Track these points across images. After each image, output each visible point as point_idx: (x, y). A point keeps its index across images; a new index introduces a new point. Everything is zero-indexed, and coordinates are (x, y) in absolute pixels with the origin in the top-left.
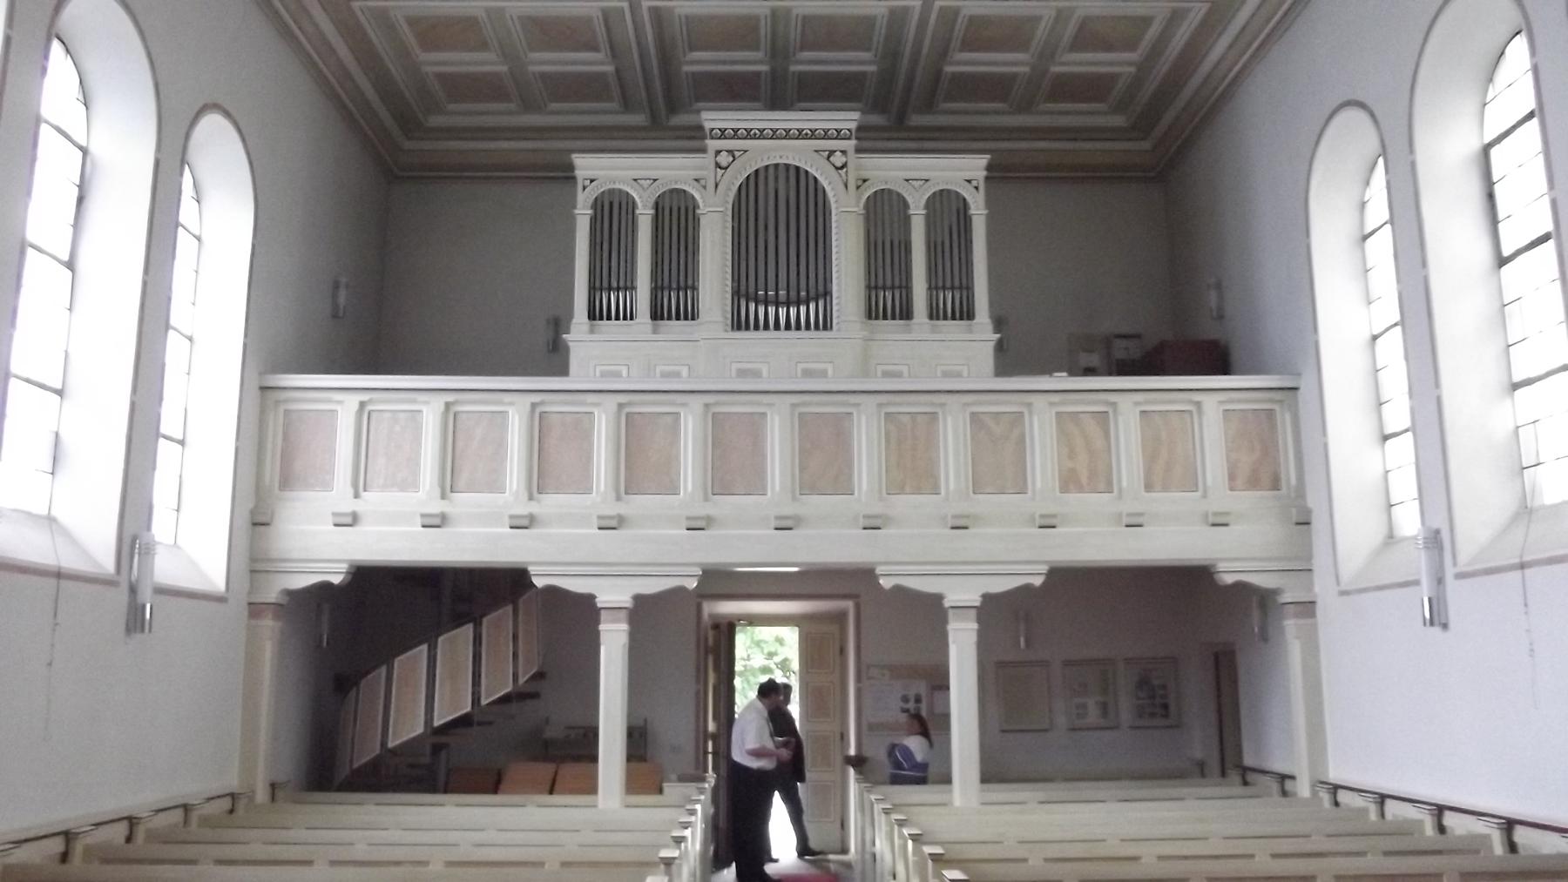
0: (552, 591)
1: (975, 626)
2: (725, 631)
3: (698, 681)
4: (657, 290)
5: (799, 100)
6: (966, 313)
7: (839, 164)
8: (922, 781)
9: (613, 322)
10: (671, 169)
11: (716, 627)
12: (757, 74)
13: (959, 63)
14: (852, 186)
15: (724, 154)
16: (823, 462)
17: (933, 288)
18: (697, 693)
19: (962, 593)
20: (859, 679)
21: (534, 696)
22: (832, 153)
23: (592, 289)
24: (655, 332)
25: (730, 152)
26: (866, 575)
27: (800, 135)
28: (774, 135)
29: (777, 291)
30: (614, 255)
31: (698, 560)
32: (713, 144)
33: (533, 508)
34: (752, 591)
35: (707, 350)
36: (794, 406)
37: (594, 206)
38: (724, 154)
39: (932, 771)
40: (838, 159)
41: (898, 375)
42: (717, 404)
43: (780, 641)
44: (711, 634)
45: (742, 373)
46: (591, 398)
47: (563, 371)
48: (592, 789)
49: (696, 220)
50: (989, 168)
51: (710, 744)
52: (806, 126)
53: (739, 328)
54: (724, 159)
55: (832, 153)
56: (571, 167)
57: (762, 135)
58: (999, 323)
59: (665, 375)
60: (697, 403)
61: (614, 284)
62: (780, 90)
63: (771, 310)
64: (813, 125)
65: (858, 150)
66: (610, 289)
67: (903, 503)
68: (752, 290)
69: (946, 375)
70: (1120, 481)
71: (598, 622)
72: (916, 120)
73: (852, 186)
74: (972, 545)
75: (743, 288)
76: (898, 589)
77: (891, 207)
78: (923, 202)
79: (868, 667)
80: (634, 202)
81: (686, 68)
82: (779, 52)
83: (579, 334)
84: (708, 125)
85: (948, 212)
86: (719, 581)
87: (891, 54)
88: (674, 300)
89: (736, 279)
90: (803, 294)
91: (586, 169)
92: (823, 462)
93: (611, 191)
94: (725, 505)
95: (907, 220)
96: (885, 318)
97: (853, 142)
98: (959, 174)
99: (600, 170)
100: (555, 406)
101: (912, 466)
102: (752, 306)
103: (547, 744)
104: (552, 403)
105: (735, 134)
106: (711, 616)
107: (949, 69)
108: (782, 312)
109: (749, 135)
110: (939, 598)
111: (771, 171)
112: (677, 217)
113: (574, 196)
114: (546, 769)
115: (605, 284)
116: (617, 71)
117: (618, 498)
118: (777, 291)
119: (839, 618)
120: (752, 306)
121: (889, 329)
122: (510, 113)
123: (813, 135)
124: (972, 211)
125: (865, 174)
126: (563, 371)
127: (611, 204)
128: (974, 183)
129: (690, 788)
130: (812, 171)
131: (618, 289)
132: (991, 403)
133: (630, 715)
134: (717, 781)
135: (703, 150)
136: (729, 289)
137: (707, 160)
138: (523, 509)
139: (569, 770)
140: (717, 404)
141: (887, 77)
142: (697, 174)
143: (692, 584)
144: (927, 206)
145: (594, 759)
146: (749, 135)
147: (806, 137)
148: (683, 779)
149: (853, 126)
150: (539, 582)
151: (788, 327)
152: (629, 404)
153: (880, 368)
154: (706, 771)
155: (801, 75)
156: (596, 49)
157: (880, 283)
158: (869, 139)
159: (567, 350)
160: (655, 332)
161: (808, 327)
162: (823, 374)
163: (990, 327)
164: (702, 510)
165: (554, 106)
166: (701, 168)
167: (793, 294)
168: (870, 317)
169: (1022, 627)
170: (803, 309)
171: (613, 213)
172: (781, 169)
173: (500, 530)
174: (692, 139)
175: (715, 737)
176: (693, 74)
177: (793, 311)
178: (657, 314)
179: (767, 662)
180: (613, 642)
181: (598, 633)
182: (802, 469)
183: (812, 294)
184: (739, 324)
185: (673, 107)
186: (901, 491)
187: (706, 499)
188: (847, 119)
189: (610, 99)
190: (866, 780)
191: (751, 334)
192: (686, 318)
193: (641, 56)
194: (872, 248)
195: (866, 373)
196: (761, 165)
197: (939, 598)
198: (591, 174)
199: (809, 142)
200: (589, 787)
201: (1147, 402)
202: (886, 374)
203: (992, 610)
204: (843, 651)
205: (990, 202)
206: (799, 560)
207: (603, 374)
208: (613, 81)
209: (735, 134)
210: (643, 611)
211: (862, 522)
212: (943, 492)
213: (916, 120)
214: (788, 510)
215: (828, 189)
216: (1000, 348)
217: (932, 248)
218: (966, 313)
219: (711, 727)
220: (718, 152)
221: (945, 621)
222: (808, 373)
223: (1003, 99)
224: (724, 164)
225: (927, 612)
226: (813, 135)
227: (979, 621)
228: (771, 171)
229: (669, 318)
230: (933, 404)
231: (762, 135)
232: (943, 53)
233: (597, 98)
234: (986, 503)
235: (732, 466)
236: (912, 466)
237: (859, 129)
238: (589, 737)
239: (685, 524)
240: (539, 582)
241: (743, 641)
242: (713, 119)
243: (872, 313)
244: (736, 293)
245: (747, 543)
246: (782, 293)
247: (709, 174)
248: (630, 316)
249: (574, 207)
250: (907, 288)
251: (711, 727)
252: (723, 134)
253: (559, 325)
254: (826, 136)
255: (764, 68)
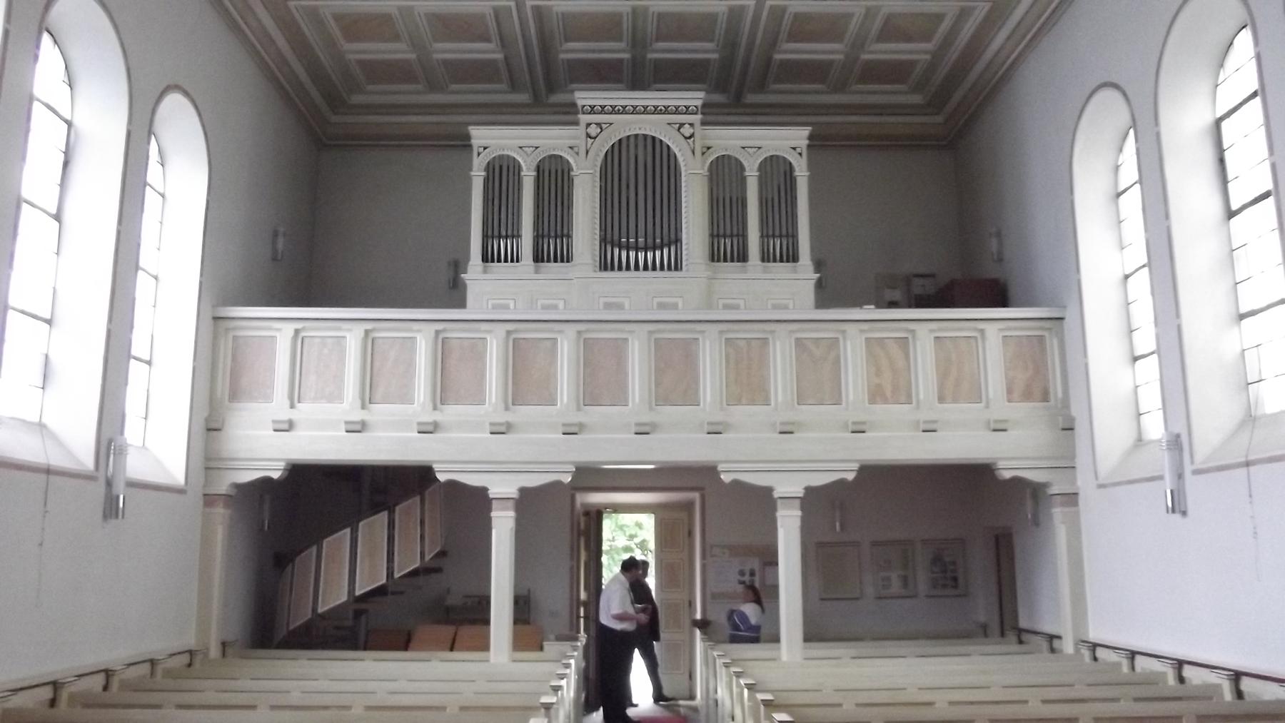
0: (452, 484)
1: (799, 513)
2: (594, 518)
3: (572, 558)
4: (538, 238)
5: (655, 82)
6: (792, 257)
7: (687, 135)
8: (755, 640)
9: (503, 264)
10: (549, 139)
11: (587, 514)
12: (621, 61)
13: (786, 52)
14: (698, 152)
15: (593, 126)
16: (675, 379)
17: (764, 236)
18: (572, 568)
19: (789, 486)
20: (704, 557)
21: (438, 570)
22: (682, 125)
23: (485, 237)
24: (537, 272)
25: (598, 124)
26: (710, 471)
27: (656, 111)
28: (635, 111)
29: (637, 239)
30: (503, 209)
31: (572, 459)
32: (584, 118)
33: (437, 416)
34: (616, 484)
35: (579, 287)
36: (650, 332)
37: (487, 169)
38: (593, 126)
39: (764, 632)
40: (687, 131)
41: (736, 307)
42: (587, 331)
43: (639, 525)
44: (582, 519)
45: (608, 306)
46: (484, 326)
47: (461, 304)
48: (485, 647)
49: (571, 180)
50: (811, 138)
51: (582, 610)
52: (661, 103)
53: (606, 269)
54: (593, 130)
55: (682, 125)
56: (468, 137)
57: (624, 111)
58: (819, 265)
59: (545, 307)
60: (571, 330)
61: (504, 233)
62: (639, 74)
63: (632, 254)
64: (666, 103)
65: (703, 123)
66: (500, 237)
67: (740, 413)
68: (616, 238)
69: (775, 307)
70: (918, 394)
71: (490, 510)
72: (751, 98)
73: (698, 152)
74: (796, 446)
75: (609, 236)
76: (736, 483)
77: (730, 169)
78: (757, 165)
79: (712, 547)
80: (520, 166)
81: (562, 56)
82: (639, 43)
83: (474, 274)
84: (580, 103)
85: (777, 173)
86: (589, 477)
87: (730, 44)
88: (552, 246)
89: (603, 229)
90: (658, 241)
91: (480, 138)
92: (675, 379)
93: (501, 157)
94: (594, 414)
95: (743, 180)
96: (725, 260)
97: (699, 117)
98: (786, 142)
99: (492, 140)
100: (455, 333)
101: (747, 382)
102: (616, 251)
103: (448, 610)
104: (452, 330)
105: (603, 110)
106: (582, 505)
107: (778, 57)
108: (641, 255)
109: (614, 110)
110: (769, 490)
111: (632, 140)
112: (554, 178)
113: (471, 160)
114: (448, 631)
115: (496, 233)
116: (506, 58)
117: (507, 409)
118: (637, 239)
119: (688, 507)
120: (616, 251)
121: (729, 269)
122: (418, 93)
123: (666, 111)
124: (797, 173)
125: (709, 143)
126: (461, 304)
127: (501, 167)
128: (799, 150)
129: (565, 646)
130: (665, 140)
131: (507, 237)
132: (812, 331)
133: (516, 586)
134: (588, 640)
135: (576, 123)
136: (597, 237)
137: (580, 131)
138: (429, 417)
139: (466, 632)
140: (587, 331)
141: (727, 63)
142: (571, 142)
143: (567, 479)
144: (760, 169)
145: (487, 622)
146: (614, 110)
147: (661, 113)
148: (560, 638)
149: (699, 103)
150: (442, 477)
151: (646, 268)
152: (516, 331)
153: (721, 302)
154: (578, 632)
155: (657, 61)
156: (488, 40)
157: (721, 232)
158: (712, 114)
159: (465, 287)
160: (537, 272)
161: (662, 268)
162: (674, 307)
163: (811, 268)
164: (575, 418)
165: (454, 87)
166: (575, 138)
167: (650, 241)
168: (713, 260)
169: (838, 514)
170: (658, 253)
171: (502, 174)
172: (640, 139)
173: (409, 434)
174: (567, 114)
175: (586, 604)
176: (568, 60)
177: (650, 255)
178: (538, 258)
179: (628, 543)
180: (503, 526)
181: (490, 519)
182: (657, 385)
183: (666, 241)
184: (606, 265)
185: (552, 88)
186: (739, 402)
187: (579, 409)
188: (695, 98)
189: (500, 81)
190: (710, 639)
191: (616, 274)
192: (562, 261)
193: (526, 46)
194: (715, 203)
195: (710, 306)
196: (623, 135)
197: (769, 490)
198: (484, 142)
199: (663, 116)
200: (483, 645)
201: (940, 330)
202: (726, 307)
203: (813, 500)
204: (690, 533)
205: (811, 166)
206: (655, 459)
207: (495, 307)
208: (502, 66)
209: (603, 110)
210: (527, 501)
211: (706, 428)
212: (773, 403)
213: (751, 98)
214: (646, 418)
215: (678, 155)
216: (819, 285)
217: (764, 203)
218: (792, 257)
219: (583, 596)
220: (589, 125)
221: (774, 509)
222: (662, 306)
223: (822, 81)
224: (593, 134)
225: (760, 502)
226: (666, 111)
227: (802, 509)
228: (632, 140)
229: (549, 261)
230: (764, 331)
231: (624, 111)
232: (773, 44)
233: (490, 80)
234: (808, 412)
235: (600, 382)
236: (747, 382)
237: (704, 106)
238: (482, 604)
239: (562, 429)
240: (442, 477)
241: (609, 525)
242: (584, 98)
243: (715, 257)
244: (603, 240)
245: (612, 445)
246: (641, 240)
247: (581, 143)
248: (516, 259)
249: (471, 170)
250: (743, 236)
251: (583, 596)
252: (592, 110)
253: (458, 266)
254: (677, 111)
255: (626, 56)
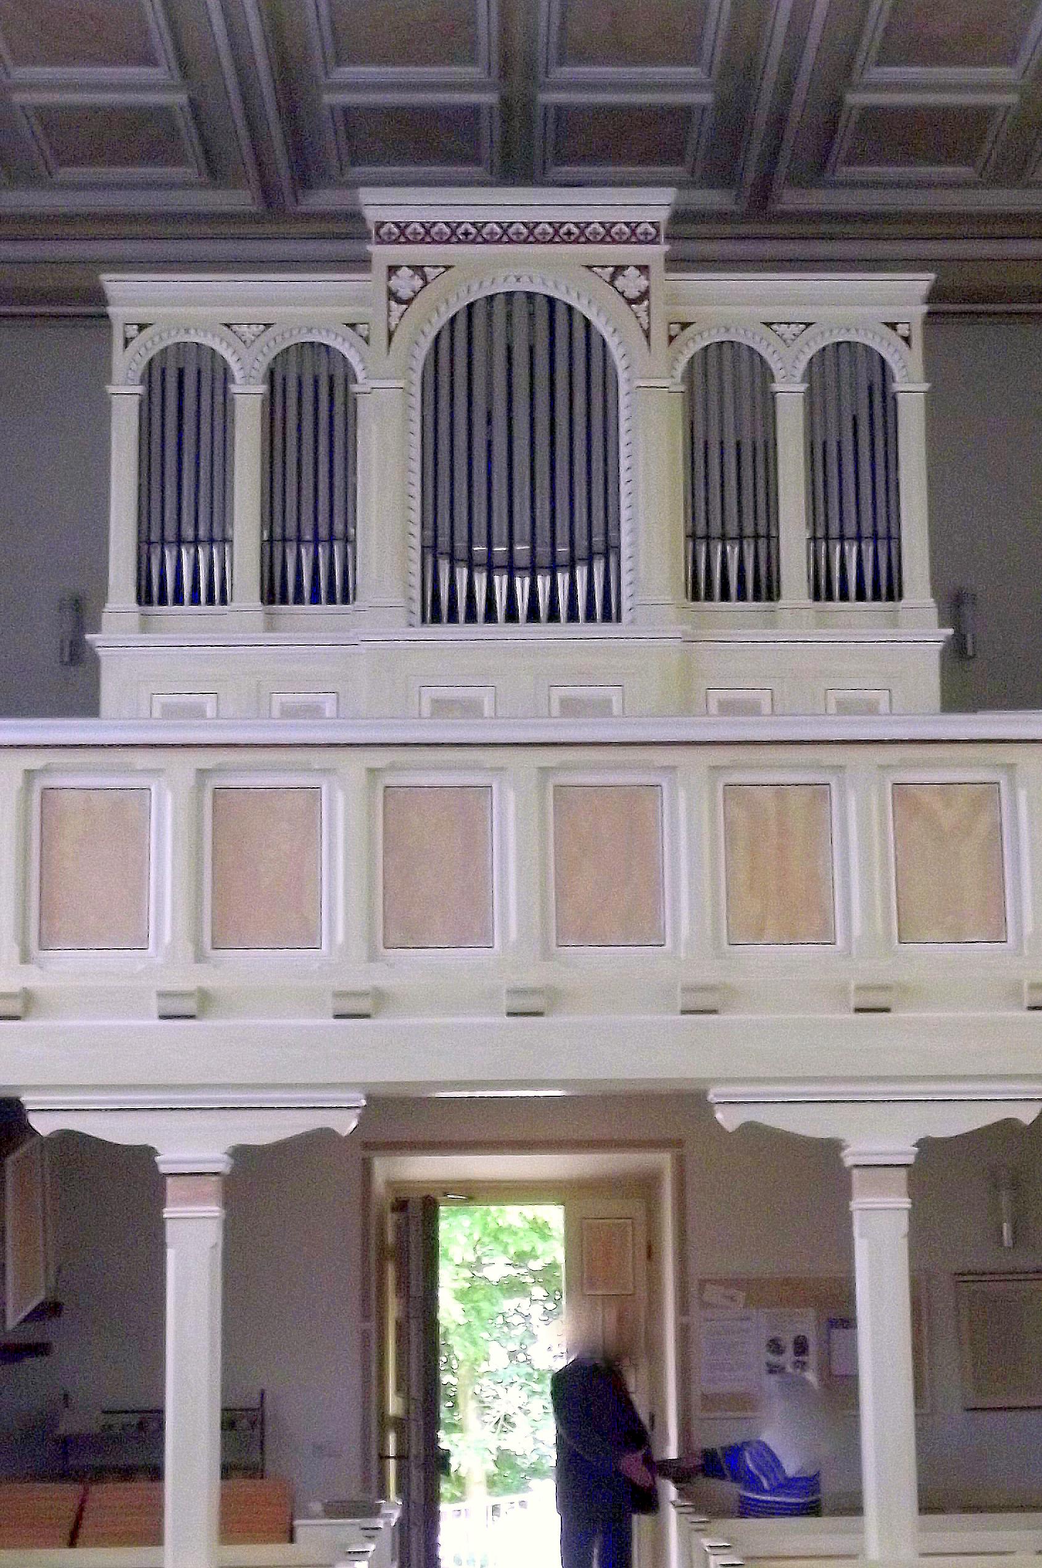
0: (70, 1142)
1: (906, 1203)
2: (419, 1213)
3: (366, 1317)
4: (272, 545)
6: (888, 587)
7: (632, 293)
8: (812, 1509)
9: (187, 608)
10: (303, 304)
11: (401, 1206)
12: (475, 111)
13: (876, 87)
14: (659, 334)
15: (405, 272)
17: (820, 537)
18: (365, 1336)
19: (880, 1138)
20: (683, 1308)
21: (40, 1349)
22: (619, 269)
23: (144, 544)
24: (270, 627)
25: (418, 269)
26: (690, 1103)
27: (559, 235)
28: (505, 235)
29: (490, 545)
31: (359, 1079)
32: (382, 254)
33: (379, 977)
34: (474, 1135)
35: (374, 662)
37: (147, 378)
38: (405, 272)
39: (829, 1487)
40: (632, 282)
41: (752, 709)
42: (393, 767)
43: (541, 1229)
44: (391, 1219)
45: (441, 707)
46: (142, 759)
47: (88, 705)
48: (153, 1536)
49: (351, 403)
50: (935, 295)
51: (392, 1439)
52: (414, 216)
53: (436, 618)
54: (405, 282)
55: (619, 269)
56: (99, 297)
57: (476, 235)
58: (955, 605)
59: (289, 712)
60: (355, 764)
61: (188, 532)
62: (524, 143)
63: (500, 582)
64: (582, 216)
65: (674, 263)
66: (180, 541)
67: (764, 960)
68: (461, 545)
69: (844, 708)
71: (162, 1203)
72: (791, 199)
73: (659, 334)
74: (890, 1043)
75: (444, 541)
76: (750, 1129)
77: (736, 379)
78: (802, 365)
79: (703, 1283)
80: (226, 370)
81: (328, 99)
82: (514, 66)
83: (120, 632)
84: (372, 215)
85: (852, 384)
86: (400, 1118)
87: (740, 72)
88: (306, 571)
90: (563, 550)
91: (132, 303)
92: (604, 878)
93: (180, 346)
94: (410, 969)
95: (767, 405)
96: (725, 596)
97: (662, 249)
98: (875, 310)
99: (157, 307)
100: (75, 776)
101: (779, 892)
102: (462, 574)
103: (66, 1444)
104: (239, 769)
105: (428, 235)
106: (390, 1184)
107: (855, 99)
108: (522, 586)
109: (455, 235)
111: (499, 307)
112: (312, 399)
113: (106, 355)
114: (60, 1497)
115: (170, 534)
117: (200, 957)
118: (490, 545)
119: (645, 1186)
120: (462, 574)
122: (186, 185)
123: (580, 235)
124: (898, 385)
125: (685, 313)
126: (88, 705)
127: (181, 373)
128: (903, 329)
129: (348, 1529)
130: (580, 306)
131: (196, 542)
132: (596, 767)
133: (225, 1390)
134: (406, 1508)
135: (363, 263)
136: (416, 542)
137: (373, 283)
138: (187, 978)
139: (107, 1496)
141: (733, 120)
142: (350, 312)
144: (808, 375)
145: (156, 1473)
146: (455, 235)
147: (569, 239)
148: (338, 1509)
149: (662, 215)
150: (728, 1119)
151: (533, 615)
152: (219, 770)
153: (715, 696)
154: (383, 1493)
155: (869, 112)
156: (148, 59)
158: (693, 242)
159: (96, 660)
160: (270, 627)
161: (573, 617)
162: (603, 709)
163: (933, 615)
164: (363, 977)
165: (65, 173)
166: (361, 301)
167: (543, 550)
168: (695, 597)
169: (1005, 1199)
170: (563, 579)
171: (183, 390)
172: (520, 303)
173: (319, 1022)
174: (343, 242)
175: (400, 1425)
176: (559, 108)
178: (273, 592)
179: (513, 1272)
180: (192, 1245)
181: (161, 1223)
182: (561, 894)
184: (436, 611)
185: (305, 177)
186: (757, 935)
187: (372, 957)
188: (653, 205)
189: (179, 160)
190: (698, 1510)
191: (461, 630)
192: (332, 600)
193: (240, 71)
194: (698, 454)
195: (686, 708)
196: (478, 294)
197: (833, 1147)
198: (142, 313)
199: (578, 243)
200: (149, 1531)
201: (905, 765)
202: (727, 708)
203: (937, 1170)
204: (651, 1252)
205: (931, 371)
206: (570, 1074)
207: (169, 712)
208: (184, 121)
209: (428, 235)
210: (254, 1180)
212: (1011, 938)
213: (791, 199)
214: (531, 978)
215: (612, 342)
216: (957, 653)
217: (817, 455)
218: (888, 587)
219: (394, 1405)
220: (393, 270)
221: (846, 1193)
222: (570, 708)
223: (968, 159)
224: (405, 293)
225: (817, 1174)
226: (580, 235)
227: (227, 1203)
228: (499, 307)
229: (299, 600)
230: (819, 767)
231: (476, 235)
232: (846, 70)
233: (152, 155)
234: (925, 960)
235: (425, 885)
236: (779, 892)
237: (679, 217)
238: (149, 1424)
239: (331, 1005)
240: (43, 1125)
241: (457, 1232)
242: (381, 204)
243: (701, 587)
244: (431, 549)
245: (448, 1045)
246: (500, 549)
247: (376, 314)
248: (216, 594)
251: (394, 1405)
252: (402, 234)
253: (81, 611)
254: (608, 235)
255: (489, 98)
